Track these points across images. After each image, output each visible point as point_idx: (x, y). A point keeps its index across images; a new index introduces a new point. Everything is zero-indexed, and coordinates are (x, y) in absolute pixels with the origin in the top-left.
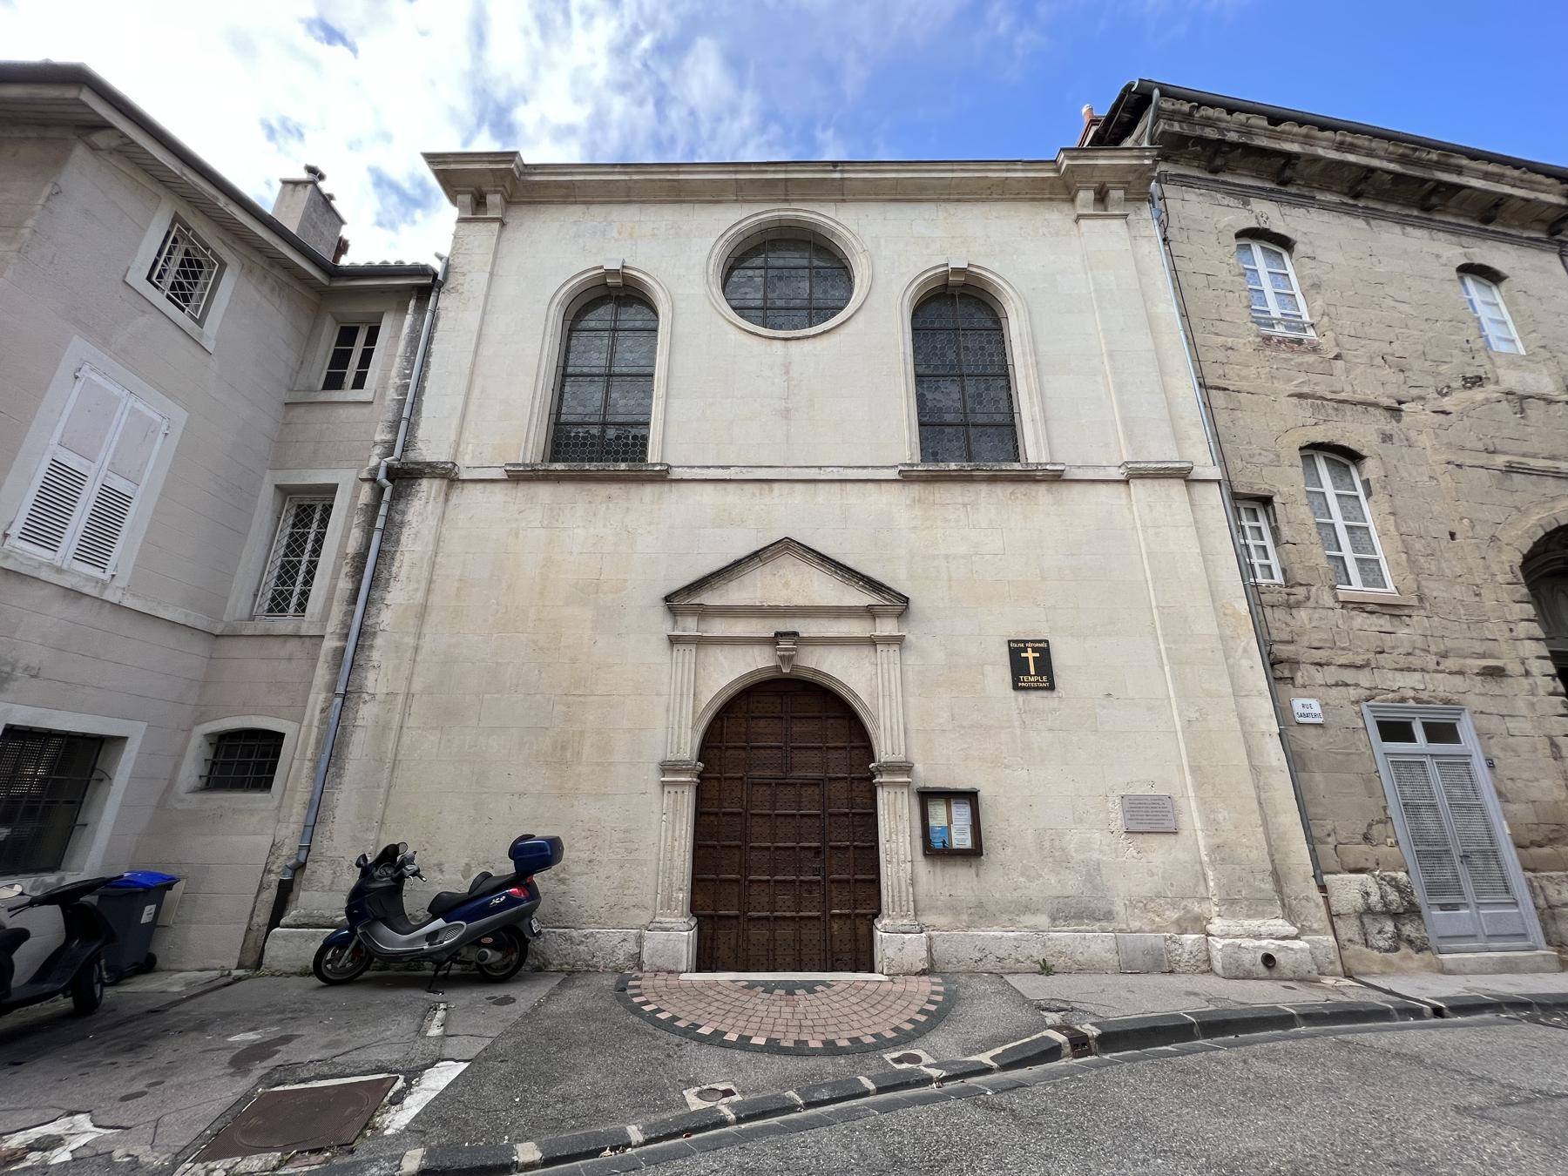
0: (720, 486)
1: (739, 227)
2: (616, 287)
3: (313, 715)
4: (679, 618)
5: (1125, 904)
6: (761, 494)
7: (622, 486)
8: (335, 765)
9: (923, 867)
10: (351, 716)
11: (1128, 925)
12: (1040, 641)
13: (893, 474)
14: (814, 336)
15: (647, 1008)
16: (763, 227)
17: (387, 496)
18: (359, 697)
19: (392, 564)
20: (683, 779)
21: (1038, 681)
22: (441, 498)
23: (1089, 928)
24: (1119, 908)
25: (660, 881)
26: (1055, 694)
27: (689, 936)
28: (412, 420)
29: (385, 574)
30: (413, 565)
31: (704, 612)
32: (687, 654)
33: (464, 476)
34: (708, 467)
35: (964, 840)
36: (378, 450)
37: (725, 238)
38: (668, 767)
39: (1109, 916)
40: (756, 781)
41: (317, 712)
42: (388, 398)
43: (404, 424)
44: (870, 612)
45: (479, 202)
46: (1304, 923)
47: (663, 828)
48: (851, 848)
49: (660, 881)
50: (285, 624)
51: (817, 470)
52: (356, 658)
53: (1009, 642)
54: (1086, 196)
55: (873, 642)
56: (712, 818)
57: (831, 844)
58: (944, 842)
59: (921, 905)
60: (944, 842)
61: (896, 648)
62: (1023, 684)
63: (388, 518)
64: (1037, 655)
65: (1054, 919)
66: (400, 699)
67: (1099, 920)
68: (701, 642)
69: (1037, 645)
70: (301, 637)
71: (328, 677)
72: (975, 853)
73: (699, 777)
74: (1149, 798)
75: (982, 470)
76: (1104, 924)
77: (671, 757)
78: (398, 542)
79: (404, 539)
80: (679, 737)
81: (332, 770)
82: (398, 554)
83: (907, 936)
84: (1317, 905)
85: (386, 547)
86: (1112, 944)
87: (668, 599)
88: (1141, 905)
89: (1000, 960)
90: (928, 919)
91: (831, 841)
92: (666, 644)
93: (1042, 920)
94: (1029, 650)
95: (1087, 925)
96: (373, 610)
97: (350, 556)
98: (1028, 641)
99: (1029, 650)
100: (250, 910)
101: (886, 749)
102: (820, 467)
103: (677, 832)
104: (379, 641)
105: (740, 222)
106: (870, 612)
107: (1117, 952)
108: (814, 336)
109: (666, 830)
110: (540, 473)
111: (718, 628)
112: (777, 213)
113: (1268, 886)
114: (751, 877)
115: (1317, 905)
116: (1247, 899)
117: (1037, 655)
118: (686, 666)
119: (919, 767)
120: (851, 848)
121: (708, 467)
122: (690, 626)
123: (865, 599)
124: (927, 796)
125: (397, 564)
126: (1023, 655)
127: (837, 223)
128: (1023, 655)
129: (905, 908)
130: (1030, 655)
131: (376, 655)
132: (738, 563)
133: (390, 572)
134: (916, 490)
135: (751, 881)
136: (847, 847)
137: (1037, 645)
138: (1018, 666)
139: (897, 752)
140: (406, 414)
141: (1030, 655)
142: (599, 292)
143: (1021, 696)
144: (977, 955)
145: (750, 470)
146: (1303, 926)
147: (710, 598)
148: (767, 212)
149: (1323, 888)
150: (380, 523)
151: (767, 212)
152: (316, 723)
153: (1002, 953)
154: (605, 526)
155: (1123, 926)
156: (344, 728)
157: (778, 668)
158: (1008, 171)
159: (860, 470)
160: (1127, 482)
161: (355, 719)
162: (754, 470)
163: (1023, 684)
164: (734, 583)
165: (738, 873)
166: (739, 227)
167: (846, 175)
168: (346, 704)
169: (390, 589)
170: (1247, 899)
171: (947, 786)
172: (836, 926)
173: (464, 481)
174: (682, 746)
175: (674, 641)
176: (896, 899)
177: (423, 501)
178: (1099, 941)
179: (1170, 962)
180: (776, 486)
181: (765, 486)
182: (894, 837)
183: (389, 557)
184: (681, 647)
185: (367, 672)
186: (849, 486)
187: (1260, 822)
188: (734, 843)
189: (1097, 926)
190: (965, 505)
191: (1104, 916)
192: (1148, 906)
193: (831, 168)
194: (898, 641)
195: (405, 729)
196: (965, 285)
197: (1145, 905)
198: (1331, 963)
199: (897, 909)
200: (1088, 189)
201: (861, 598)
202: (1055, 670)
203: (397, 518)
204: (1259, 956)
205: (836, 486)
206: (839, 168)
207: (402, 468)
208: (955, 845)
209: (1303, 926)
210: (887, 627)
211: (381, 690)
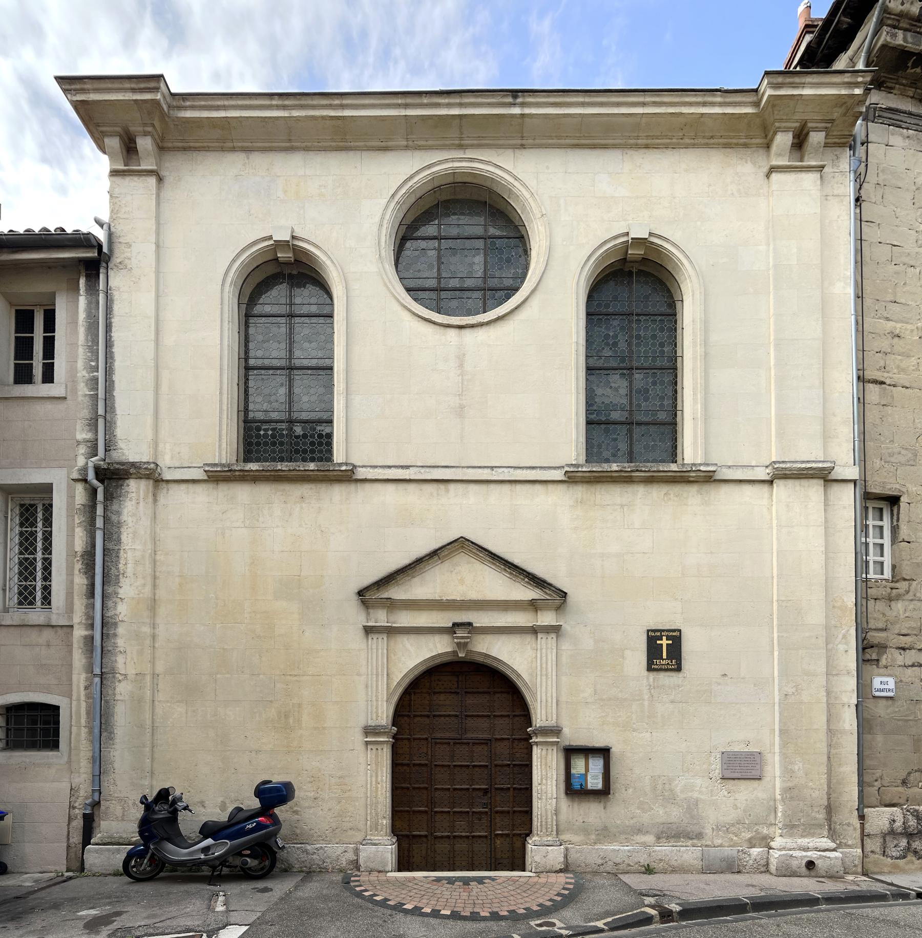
0: (401, 486)
1: (410, 184)
2: (287, 264)
3: (79, 692)
4: (371, 611)
5: (713, 828)
6: (438, 495)
7: (312, 486)
8: (106, 730)
9: (564, 803)
10: (110, 692)
11: (713, 842)
12: (674, 631)
13: (558, 475)
14: (488, 323)
15: (366, 894)
16: (437, 184)
17: (100, 496)
18: (114, 677)
19: (117, 563)
20: (382, 739)
21: (668, 664)
22: (150, 499)
23: (684, 844)
24: (708, 831)
25: (369, 812)
26: (681, 675)
27: (392, 848)
28: (108, 418)
29: (113, 571)
30: (137, 563)
31: (392, 605)
32: (379, 642)
33: (167, 476)
34: (390, 467)
35: (597, 784)
36: (82, 450)
37: (397, 198)
38: (369, 731)
39: (699, 836)
40: (438, 741)
41: (82, 688)
42: (80, 393)
43: (101, 422)
44: (533, 606)
45: (130, 149)
46: (843, 841)
47: (369, 775)
48: (512, 789)
49: (369, 812)
50: (36, 615)
51: (489, 470)
52: (104, 645)
53: (648, 631)
54: (783, 140)
55: (534, 631)
56: (405, 768)
57: (496, 786)
58: (581, 785)
59: (562, 827)
60: (581, 785)
61: (554, 635)
62: (656, 667)
63: (106, 519)
64: (670, 642)
65: (658, 838)
66: (148, 678)
67: (692, 839)
68: (391, 631)
69: (671, 634)
70: (53, 626)
71: (84, 661)
72: (604, 793)
73: (393, 738)
74: (744, 754)
75: (641, 471)
76: (695, 841)
77: (370, 723)
78: (119, 541)
79: (124, 537)
80: (377, 708)
81: (104, 734)
82: (122, 551)
83: (550, 848)
84: (855, 829)
85: (110, 546)
86: (699, 854)
87: (360, 593)
88: (725, 828)
89: (616, 864)
90: (565, 837)
91: (496, 784)
92: (361, 633)
93: (650, 839)
94: (664, 638)
95: (683, 842)
96: (110, 604)
97: (79, 554)
98: (663, 631)
99: (664, 638)
100: (66, 833)
101: (541, 717)
102: (492, 468)
103: (379, 778)
104: (121, 630)
105: (411, 177)
106: (533, 606)
107: (702, 860)
108: (488, 323)
109: (371, 776)
110: (237, 473)
111: (405, 619)
112: (450, 165)
113: (821, 816)
114: (436, 809)
115: (855, 829)
116: (804, 825)
117: (670, 642)
118: (380, 651)
119: (566, 731)
120: (512, 789)
121: (390, 467)
122: (381, 618)
123: (528, 593)
124: (570, 752)
125: (122, 561)
126: (659, 642)
127: (516, 178)
128: (659, 642)
129: (550, 830)
130: (664, 642)
131: (120, 642)
132: (419, 561)
133: (118, 569)
134: (579, 491)
135: (436, 812)
136: (509, 789)
137: (671, 634)
138: (653, 651)
139: (550, 719)
140: (101, 411)
141: (664, 642)
142: (271, 270)
143: (652, 675)
144: (600, 861)
145: (428, 470)
146: (840, 842)
147: (397, 593)
148: (440, 162)
149: (862, 817)
150: (99, 523)
151: (440, 162)
152: (83, 698)
153: (618, 860)
154: (300, 526)
155: (709, 843)
156: (107, 702)
157: (455, 653)
158: (704, 104)
159: (529, 471)
160: (771, 482)
161: (114, 694)
162: (431, 470)
163: (656, 667)
164: (416, 580)
165: (426, 807)
166: (410, 184)
167: (527, 111)
168: (104, 682)
169: (121, 585)
170: (804, 825)
171: (588, 745)
172: (498, 842)
173: (168, 481)
174: (380, 715)
175: (369, 631)
176: (544, 823)
177: (134, 502)
178: (690, 853)
179: (739, 866)
180: (452, 486)
181: (442, 486)
182: (544, 781)
183: (114, 555)
184: (375, 636)
185: (116, 656)
186: (519, 487)
187: (826, 771)
188: (422, 786)
189: (690, 843)
190: (622, 506)
191: (696, 836)
192: (729, 830)
193: (510, 100)
194: (555, 630)
195: (156, 703)
196: (645, 260)
197: (728, 829)
198: (855, 866)
199: (544, 831)
200: (786, 130)
201: (525, 593)
202: (683, 655)
203: (114, 518)
204: (804, 862)
205: (506, 488)
206: (519, 100)
207: (108, 469)
208: (590, 787)
209: (840, 842)
210: (547, 618)
211: (131, 671)
